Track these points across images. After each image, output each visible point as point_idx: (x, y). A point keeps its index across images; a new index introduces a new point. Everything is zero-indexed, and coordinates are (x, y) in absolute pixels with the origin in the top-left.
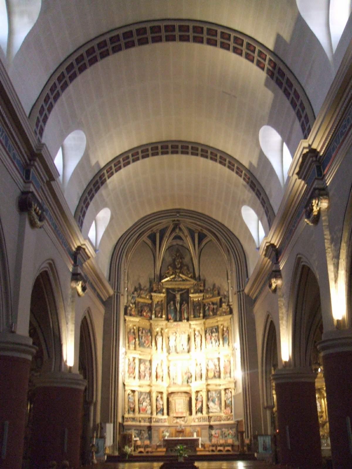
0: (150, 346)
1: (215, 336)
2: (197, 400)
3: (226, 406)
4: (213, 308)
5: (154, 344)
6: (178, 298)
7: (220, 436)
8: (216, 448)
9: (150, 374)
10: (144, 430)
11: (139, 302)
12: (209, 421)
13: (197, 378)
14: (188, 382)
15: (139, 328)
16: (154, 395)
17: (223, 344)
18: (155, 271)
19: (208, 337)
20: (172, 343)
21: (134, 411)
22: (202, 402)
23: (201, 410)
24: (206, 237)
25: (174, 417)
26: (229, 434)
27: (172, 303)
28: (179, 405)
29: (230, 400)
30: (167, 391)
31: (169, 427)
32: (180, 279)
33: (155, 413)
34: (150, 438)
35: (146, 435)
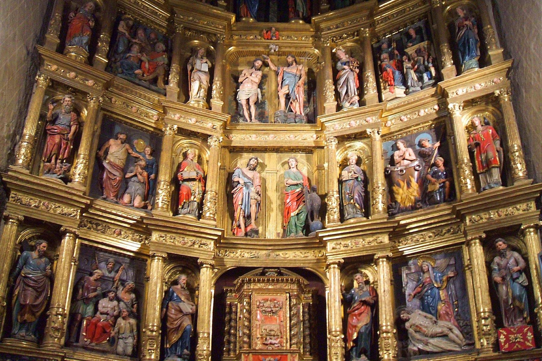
1: (419, 52)
2: (347, 302)
5: (174, 80)
13: (349, 210)
14: (307, 229)
15: (119, 196)
16: (156, 270)
19: (388, 64)
20: (248, 91)
22: (374, 306)
24: (435, 138)
30: (219, 261)
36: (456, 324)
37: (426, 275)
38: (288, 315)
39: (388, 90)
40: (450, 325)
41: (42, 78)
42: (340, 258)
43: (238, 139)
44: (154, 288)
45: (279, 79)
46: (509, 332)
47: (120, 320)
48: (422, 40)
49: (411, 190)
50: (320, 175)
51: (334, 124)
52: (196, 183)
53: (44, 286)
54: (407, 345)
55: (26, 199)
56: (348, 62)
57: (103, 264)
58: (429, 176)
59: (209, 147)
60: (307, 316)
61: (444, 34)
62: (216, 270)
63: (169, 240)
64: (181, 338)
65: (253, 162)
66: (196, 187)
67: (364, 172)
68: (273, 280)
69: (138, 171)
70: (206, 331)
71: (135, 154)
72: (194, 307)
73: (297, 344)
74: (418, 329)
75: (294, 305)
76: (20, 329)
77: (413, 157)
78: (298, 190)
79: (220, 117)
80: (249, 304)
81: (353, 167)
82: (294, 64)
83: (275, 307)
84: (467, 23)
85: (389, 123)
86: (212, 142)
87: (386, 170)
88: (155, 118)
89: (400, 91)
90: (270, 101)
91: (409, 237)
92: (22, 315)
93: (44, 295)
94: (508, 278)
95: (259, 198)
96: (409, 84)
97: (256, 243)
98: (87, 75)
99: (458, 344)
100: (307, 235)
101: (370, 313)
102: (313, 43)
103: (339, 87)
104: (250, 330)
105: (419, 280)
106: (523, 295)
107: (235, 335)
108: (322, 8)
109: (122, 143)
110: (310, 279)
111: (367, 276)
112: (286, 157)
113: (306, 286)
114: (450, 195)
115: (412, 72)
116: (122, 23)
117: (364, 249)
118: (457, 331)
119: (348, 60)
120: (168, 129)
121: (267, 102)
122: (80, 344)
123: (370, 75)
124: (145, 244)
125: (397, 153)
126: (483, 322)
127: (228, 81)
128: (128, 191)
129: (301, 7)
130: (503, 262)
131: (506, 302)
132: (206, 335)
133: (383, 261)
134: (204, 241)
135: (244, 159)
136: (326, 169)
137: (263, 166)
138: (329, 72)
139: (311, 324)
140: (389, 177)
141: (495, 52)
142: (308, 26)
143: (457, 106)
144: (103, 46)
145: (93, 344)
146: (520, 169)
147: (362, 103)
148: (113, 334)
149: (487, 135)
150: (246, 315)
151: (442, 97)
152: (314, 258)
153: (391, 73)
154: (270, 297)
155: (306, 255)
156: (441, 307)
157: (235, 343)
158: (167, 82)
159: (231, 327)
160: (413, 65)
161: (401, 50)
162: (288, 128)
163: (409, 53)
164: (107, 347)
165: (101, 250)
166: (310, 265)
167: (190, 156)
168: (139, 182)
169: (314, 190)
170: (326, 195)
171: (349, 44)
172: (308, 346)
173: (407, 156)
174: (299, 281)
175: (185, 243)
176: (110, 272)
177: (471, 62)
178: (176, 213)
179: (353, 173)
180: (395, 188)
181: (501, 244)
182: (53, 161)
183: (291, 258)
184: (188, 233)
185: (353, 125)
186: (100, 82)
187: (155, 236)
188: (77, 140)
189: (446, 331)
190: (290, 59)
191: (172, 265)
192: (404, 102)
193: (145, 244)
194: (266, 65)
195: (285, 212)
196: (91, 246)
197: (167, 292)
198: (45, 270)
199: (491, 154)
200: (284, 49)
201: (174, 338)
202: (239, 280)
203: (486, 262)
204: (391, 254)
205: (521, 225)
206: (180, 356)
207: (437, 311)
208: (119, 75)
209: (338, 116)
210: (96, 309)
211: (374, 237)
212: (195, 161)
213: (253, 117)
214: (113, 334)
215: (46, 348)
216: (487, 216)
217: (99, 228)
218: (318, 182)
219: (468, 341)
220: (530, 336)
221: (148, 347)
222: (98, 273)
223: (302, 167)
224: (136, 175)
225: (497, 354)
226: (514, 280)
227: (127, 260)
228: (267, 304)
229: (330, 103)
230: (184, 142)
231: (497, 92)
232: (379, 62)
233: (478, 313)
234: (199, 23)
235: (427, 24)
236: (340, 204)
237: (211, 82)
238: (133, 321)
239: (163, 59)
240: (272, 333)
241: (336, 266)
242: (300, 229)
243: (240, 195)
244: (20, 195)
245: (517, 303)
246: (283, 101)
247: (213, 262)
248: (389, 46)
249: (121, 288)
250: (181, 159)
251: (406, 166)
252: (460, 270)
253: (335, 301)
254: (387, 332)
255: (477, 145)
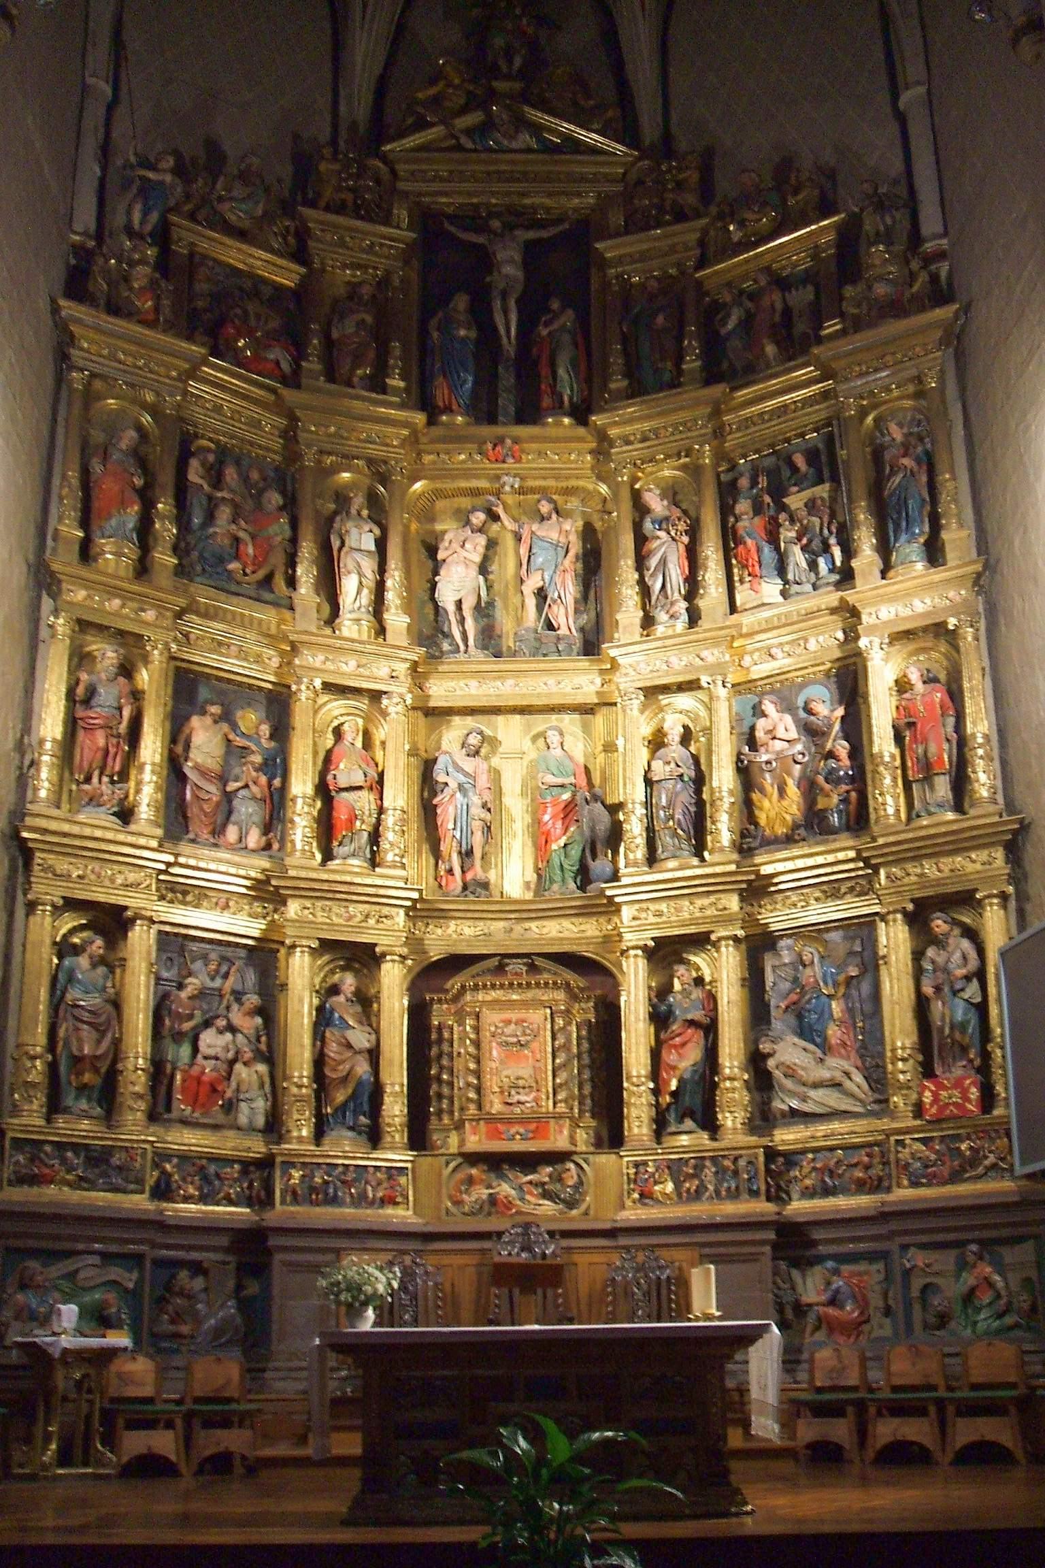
0: (280, 582)
1: (811, 506)
2: (660, 1018)
3: (930, 1047)
4: (787, 312)
5: (306, 573)
6: (509, 266)
7: (877, 1318)
8: (862, 1434)
9: (276, 807)
10: (197, 1269)
11: (194, 260)
12: (778, 1195)
13: (665, 840)
14: (584, 876)
15: (218, 831)
16: (301, 973)
17: (885, 549)
18: (335, 104)
19: (748, 524)
20: (457, 583)
21: (108, 1095)
22: (710, 1029)
23: (696, 1103)
24: (836, 697)
25: (473, 1159)
26: (969, 1298)
27: (461, 302)
28: (517, 1055)
29: (972, 991)
30: (415, 943)
31: (428, 1237)
32: (526, 139)
33: (301, 1127)
34: (253, 1335)
35: (219, 1311)
36: (859, 1064)
37: (808, 971)
38: (549, 1049)
39: (747, 585)
40: (846, 1065)
41: (61, 621)
42: (647, 937)
43: (441, 691)
44: (296, 1007)
45: (523, 551)
46: (941, 1086)
47: (238, 1067)
48: (820, 481)
49: (785, 803)
50: (610, 764)
51: (636, 658)
52: (364, 794)
53: (108, 1021)
54: (770, 1100)
55: (62, 865)
56: (667, 519)
57: (198, 966)
58: (821, 779)
59: (385, 714)
60: (586, 1045)
61: (860, 477)
62: (409, 962)
63: (320, 914)
64: (354, 1097)
65: (474, 740)
66: (364, 801)
67: (696, 759)
68: (520, 985)
69: (250, 779)
70: (398, 1080)
71: (239, 741)
72: (374, 1037)
73: (566, 1101)
74: (790, 1073)
75: (561, 1029)
76: (77, 1098)
77: (793, 734)
78: (566, 796)
79: (404, 654)
80: (477, 1029)
81: (675, 750)
82: (554, 516)
83: (524, 1034)
84: (906, 461)
85: (747, 661)
86: (393, 706)
87: (739, 760)
88: (275, 662)
89: (771, 589)
90: (505, 600)
91: (779, 897)
92: (79, 1074)
93: (110, 1035)
94: (946, 989)
95: (488, 817)
96: (790, 577)
97: (485, 907)
98: (143, 601)
99: (860, 1101)
100: (582, 888)
101: (702, 1042)
102: (592, 468)
103: (647, 574)
104: (479, 1078)
105: (795, 980)
106: (968, 1022)
107: (451, 1084)
108: (613, 386)
109: (216, 722)
110: (589, 970)
111: (698, 969)
112: (540, 723)
113: (582, 990)
114: (859, 819)
115: (797, 549)
116: (194, 463)
117: (693, 922)
118: (858, 1078)
119: (667, 513)
120: (303, 687)
121: (499, 603)
122: (174, 1114)
123: (712, 553)
124: (273, 921)
125: (761, 724)
126: (900, 1065)
127: (414, 558)
128: (233, 818)
129: (568, 386)
130: (940, 960)
131: (941, 1030)
132: (397, 1088)
133: (727, 946)
134: (386, 910)
135: (452, 735)
136: (621, 749)
137: (493, 742)
138: (627, 541)
139: (593, 1060)
140: (746, 773)
141: (957, 537)
142: (581, 431)
143: (877, 641)
144: (166, 529)
145: (196, 1115)
146: (983, 780)
147: (694, 617)
148: (229, 1094)
149: (929, 706)
150: (471, 1049)
151: (850, 614)
152: (597, 933)
153: (753, 550)
154: (514, 1015)
155: (583, 927)
156: (834, 1033)
157: (451, 1099)
158: (292, 582)
159: (441, 1068)
160: (799, 539)
161: (778, 492)
162: (542, 666)
163: (793, 507)
164: (221, 1118)
165: (194, 939)
166: (591, 948)
167: (348, 737)
168: (254, 798)
169: (596, 798)
170: (620, 806)
171: (667, 473)
172: (588, 1101)
173: (780, 733)
174: (568, 984)
175: (350, 918)
176: (213, 979)
177: (910, 551)
178: (328, 856)
179: (673, 765)
180: (756, 796)
181: (939, 924)
182: (95, 780)
183: (554, 934)
184: (355, 898)
185: (677, 665)
186: (168, 609)
187: (293, 908)
188: (134, 735)
189: (839, 1076)
190: (545, 507)
191: (326, 958)
192: (779, 616)
193: (273, 921)
194: (495, 518)
195: (541, 840)
196: (176, 934)
197: (320, 1009)
198: (104, 988)
199: (933, 749)
200: (531, 483)
201: (340, 1096)
202: (455, 983)
203: (913, 953)
204: (741, 933)
205: (976, 890)
206: (351, 1129)
207: (825, 1039)
208: (198, 579)
209: (645, 646)
210: (195, 1050)
211: (712, 899)
212: (359, 744)
213: (471, 642)
214: (229, 1094)
215: (124, 1130)
216: (918, 871)
217: (189, 898)
218: (604, 779)
219: (877, 1096)
220: (974, 1093)
221: (296, 1116)
222: (193, 984)
223: (574, 742)
224: (246, 786)
225: (918, 1122)
226: (955, 993)
227: (243, 953)
228: (510, 1029)
229: (629, 613)
230: (336, 708)
231: (952, 622)
232: (732, 519)
233: (894, 1050)
234: (347, 439)
235: (830, 440)
236: (647, 829)
237: (382, 569)
238: (262, 1068)
239: (280, 528)
240: (521, 1083)
241: (640, 952)
242: (569, 876)
243: (451, 810)
244: (51, 859)
245: (957, 1036)
246: (531, 602)
247: (405, 951)
248: (754, 483)
249: (235, 1007)
250: (329, 741)
251: (778, 753)
252: (871, 963)
253: (637, 1020)
254: (731, 1079)
255: (911, 725)
